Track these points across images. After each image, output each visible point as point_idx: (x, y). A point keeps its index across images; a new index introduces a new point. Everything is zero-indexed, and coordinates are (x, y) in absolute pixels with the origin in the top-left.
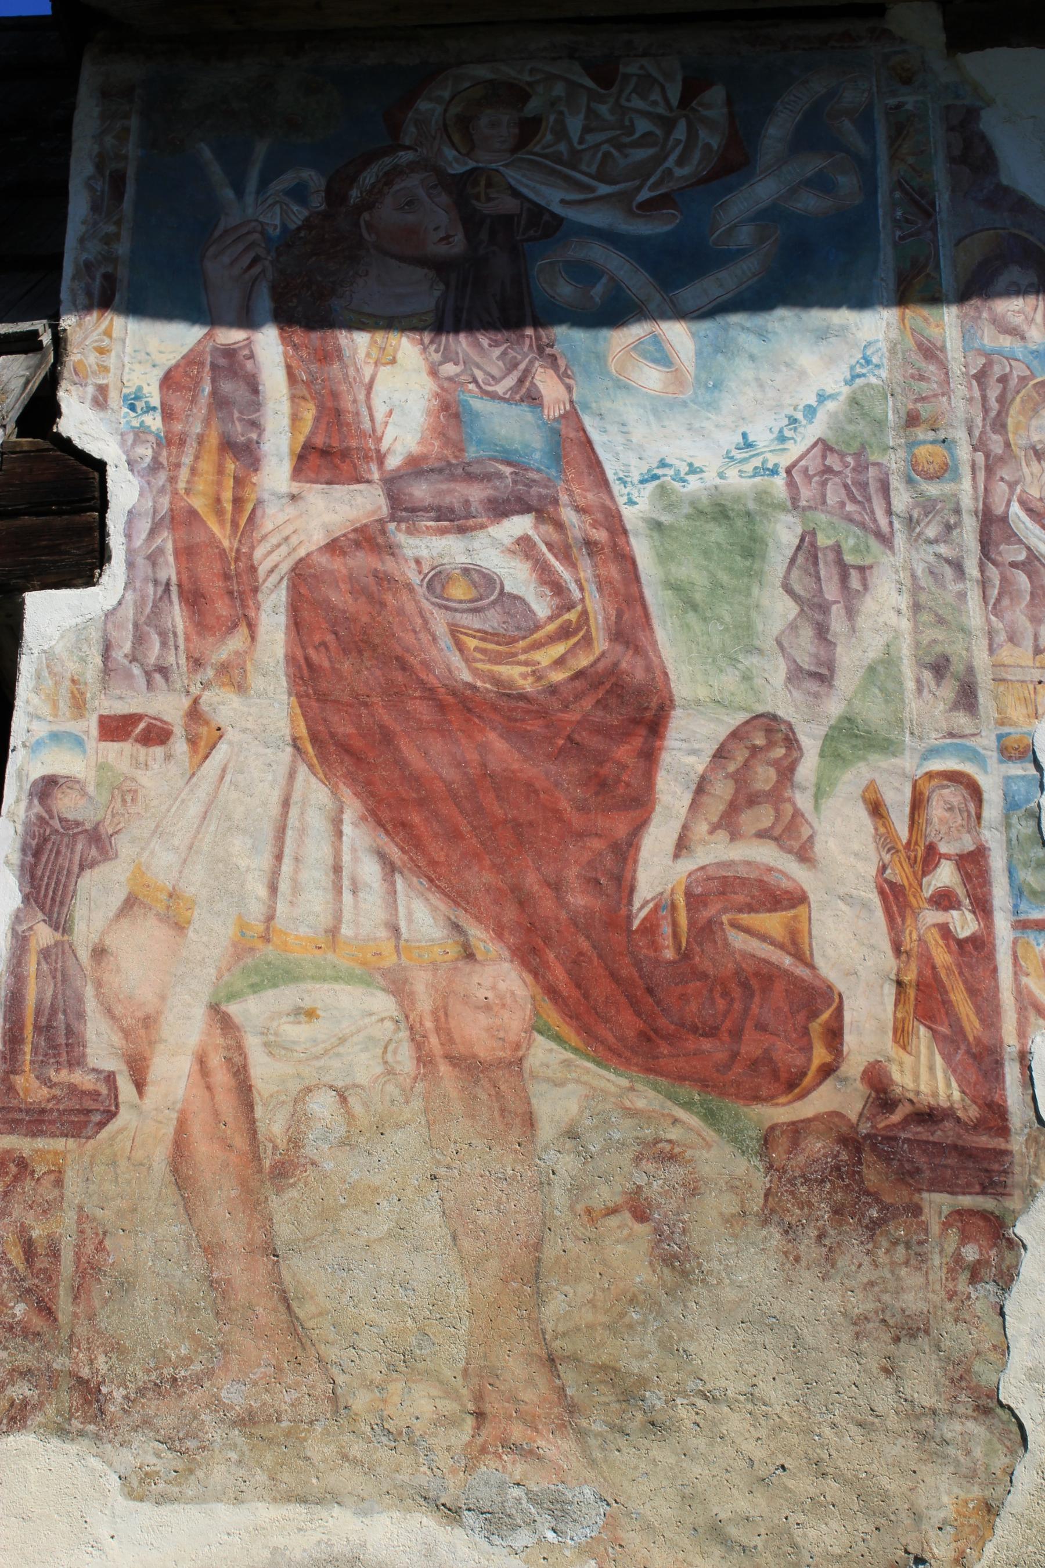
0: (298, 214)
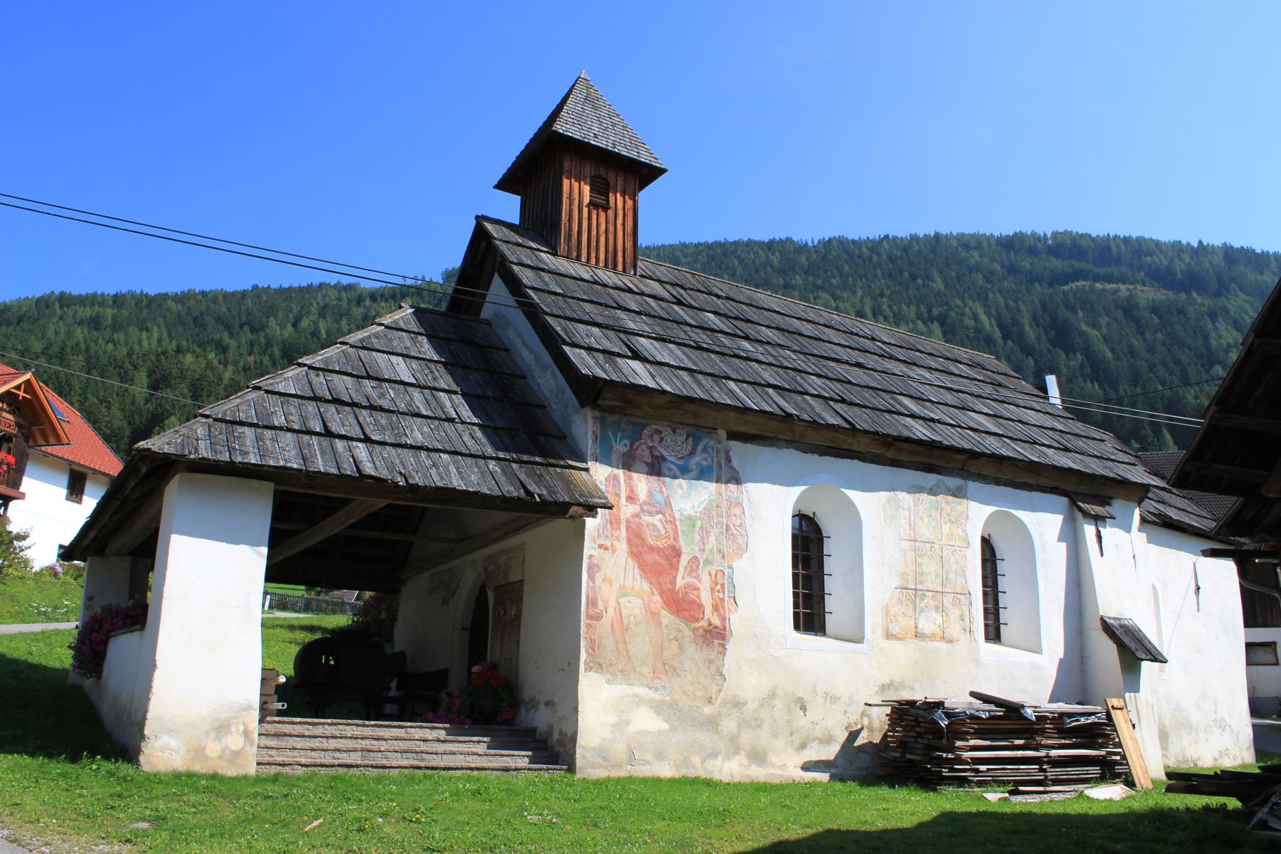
0: (625, 450)
